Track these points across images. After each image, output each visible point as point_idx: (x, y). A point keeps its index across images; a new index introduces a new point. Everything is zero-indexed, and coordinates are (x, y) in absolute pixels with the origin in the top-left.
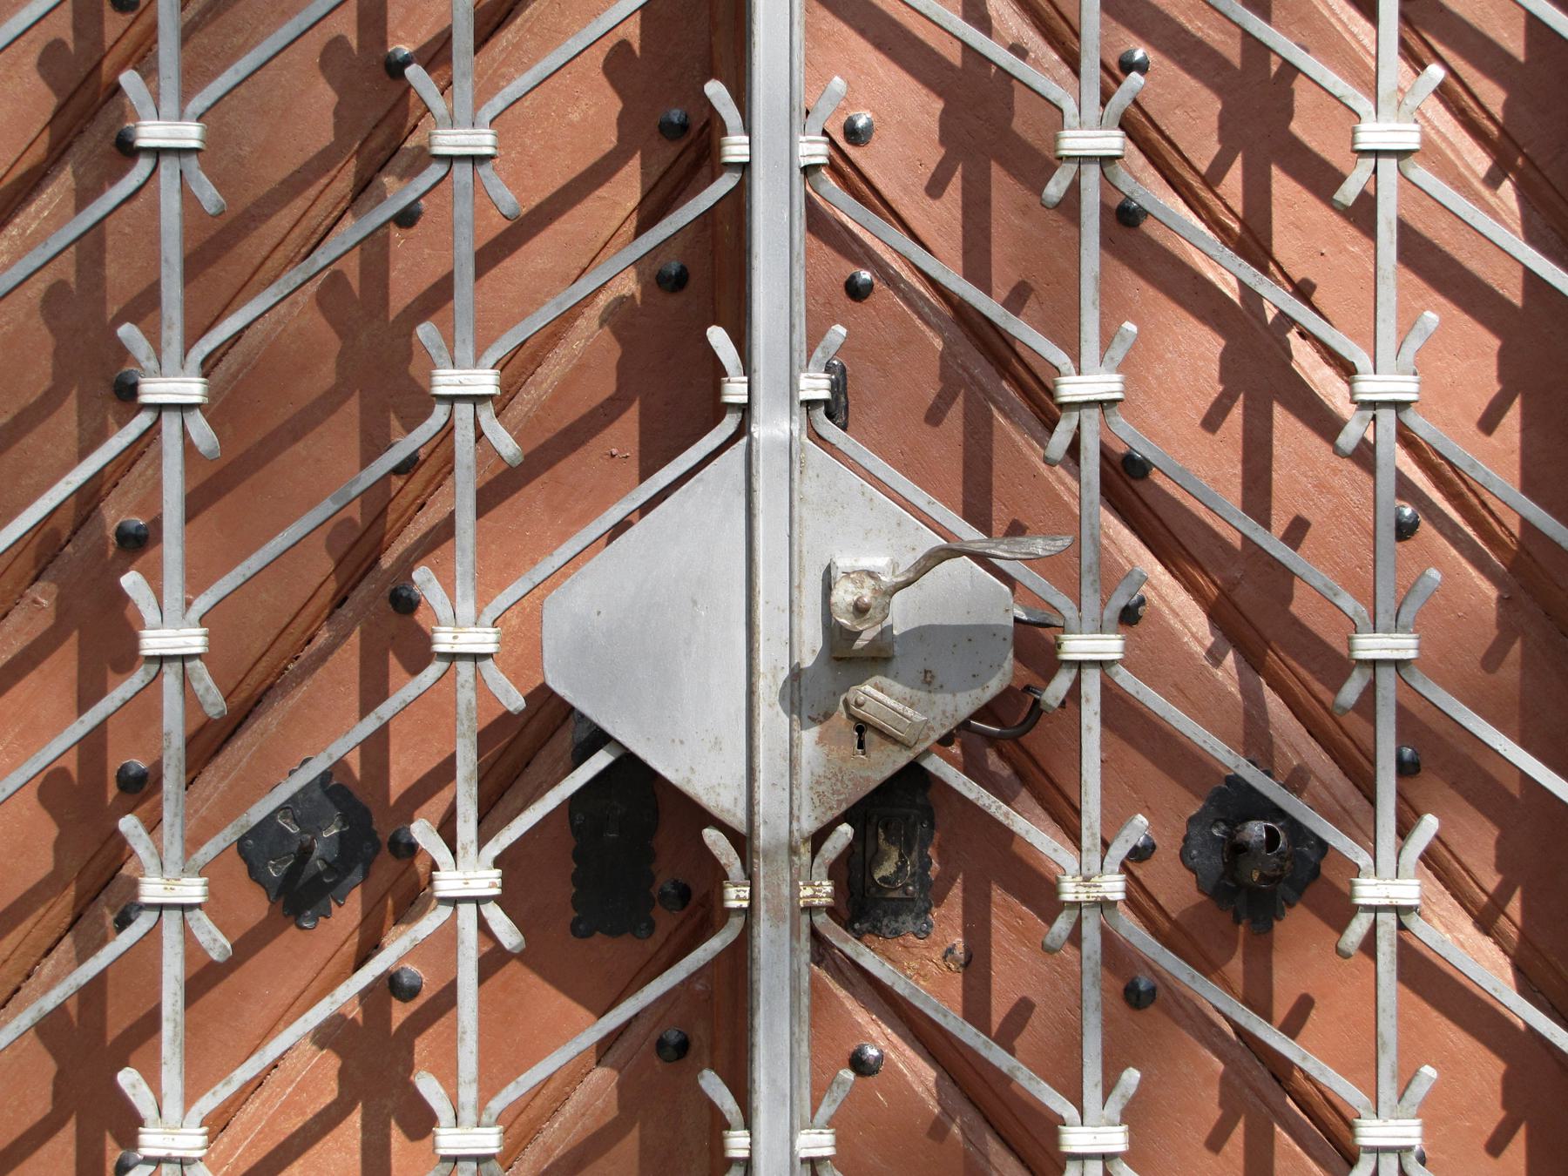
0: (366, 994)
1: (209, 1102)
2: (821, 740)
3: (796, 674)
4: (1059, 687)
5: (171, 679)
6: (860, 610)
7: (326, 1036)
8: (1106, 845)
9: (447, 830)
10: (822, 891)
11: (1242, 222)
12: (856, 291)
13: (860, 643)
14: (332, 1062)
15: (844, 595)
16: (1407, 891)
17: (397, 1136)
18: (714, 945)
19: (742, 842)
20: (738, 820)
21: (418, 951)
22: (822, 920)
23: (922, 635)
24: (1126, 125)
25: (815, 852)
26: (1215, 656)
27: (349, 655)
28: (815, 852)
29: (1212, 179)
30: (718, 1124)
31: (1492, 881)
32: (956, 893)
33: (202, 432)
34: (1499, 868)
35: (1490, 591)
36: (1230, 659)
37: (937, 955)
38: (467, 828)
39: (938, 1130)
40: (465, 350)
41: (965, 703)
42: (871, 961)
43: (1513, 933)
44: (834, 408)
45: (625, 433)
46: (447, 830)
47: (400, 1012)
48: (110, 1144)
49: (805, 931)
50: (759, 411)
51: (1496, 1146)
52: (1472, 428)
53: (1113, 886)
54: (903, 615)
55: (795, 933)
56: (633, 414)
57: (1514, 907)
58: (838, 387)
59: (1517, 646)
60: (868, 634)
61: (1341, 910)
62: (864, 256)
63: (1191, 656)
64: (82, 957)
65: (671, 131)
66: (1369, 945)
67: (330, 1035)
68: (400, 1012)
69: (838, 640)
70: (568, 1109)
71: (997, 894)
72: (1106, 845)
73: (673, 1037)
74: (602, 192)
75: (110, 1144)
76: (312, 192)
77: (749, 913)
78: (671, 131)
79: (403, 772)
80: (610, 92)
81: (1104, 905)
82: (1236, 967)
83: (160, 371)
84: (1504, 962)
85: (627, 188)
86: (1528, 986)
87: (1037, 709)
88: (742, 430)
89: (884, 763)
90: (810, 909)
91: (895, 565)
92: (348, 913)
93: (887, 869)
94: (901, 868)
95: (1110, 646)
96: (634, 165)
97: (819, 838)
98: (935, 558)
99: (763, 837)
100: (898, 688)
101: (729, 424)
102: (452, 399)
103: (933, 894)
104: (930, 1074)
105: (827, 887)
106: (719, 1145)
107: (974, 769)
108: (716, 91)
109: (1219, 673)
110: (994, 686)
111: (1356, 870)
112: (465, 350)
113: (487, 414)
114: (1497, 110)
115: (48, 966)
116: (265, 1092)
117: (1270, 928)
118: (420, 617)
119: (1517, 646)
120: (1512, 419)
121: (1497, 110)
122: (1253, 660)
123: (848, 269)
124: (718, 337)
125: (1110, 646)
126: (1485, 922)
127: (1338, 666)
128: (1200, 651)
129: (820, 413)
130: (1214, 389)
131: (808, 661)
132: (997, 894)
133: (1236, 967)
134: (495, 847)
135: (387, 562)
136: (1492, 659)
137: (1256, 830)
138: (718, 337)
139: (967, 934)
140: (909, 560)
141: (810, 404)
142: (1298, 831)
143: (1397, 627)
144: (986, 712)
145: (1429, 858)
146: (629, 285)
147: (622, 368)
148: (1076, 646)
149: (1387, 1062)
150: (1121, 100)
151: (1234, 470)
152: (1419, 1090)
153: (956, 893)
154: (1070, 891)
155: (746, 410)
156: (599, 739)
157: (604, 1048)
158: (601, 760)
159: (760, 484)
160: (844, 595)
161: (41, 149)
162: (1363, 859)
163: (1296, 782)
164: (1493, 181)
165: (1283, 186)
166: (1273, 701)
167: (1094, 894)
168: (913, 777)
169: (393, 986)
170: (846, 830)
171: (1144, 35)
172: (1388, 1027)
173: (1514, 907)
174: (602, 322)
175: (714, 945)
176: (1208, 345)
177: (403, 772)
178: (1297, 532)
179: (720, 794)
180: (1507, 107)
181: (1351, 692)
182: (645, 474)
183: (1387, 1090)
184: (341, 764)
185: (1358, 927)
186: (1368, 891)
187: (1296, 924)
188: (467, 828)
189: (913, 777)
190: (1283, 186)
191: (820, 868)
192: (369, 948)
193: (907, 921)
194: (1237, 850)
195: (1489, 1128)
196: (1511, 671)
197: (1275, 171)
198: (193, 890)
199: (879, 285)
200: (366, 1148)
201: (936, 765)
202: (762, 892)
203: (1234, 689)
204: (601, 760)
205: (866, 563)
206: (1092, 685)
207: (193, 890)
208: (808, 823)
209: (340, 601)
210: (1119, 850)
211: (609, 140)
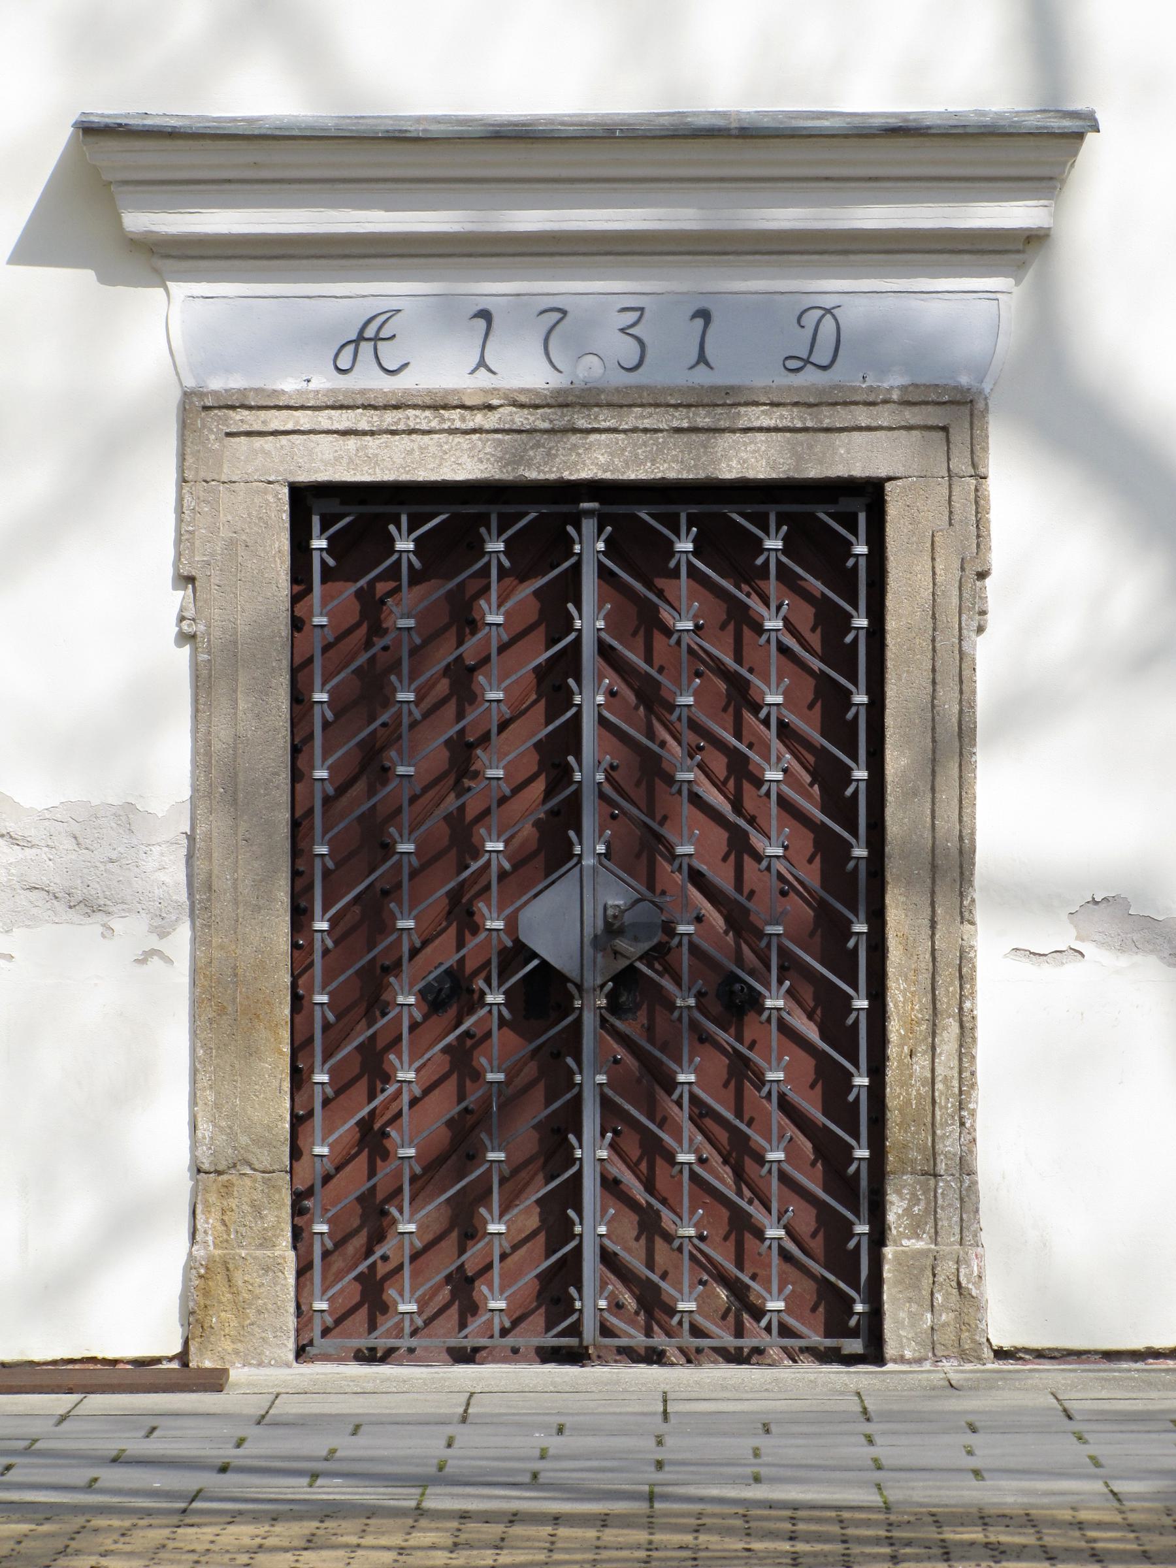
0: (459, 1038)
1: (417, 1064)
2: (603, 956)
3: (596, 936)
4: (676, 941)
5: (405, 936)
6: (615, 917)
7: (445, 1050)
8: (690, 989)
9: (488, 981)
10: (603, 1002)
11: (734, 796)
12: (614, 817)
13: (615, 927)
14: (447, 1058)
15: (610, 912)
16: (780, 1003)
17: (468, 1083)
18: (570, 1019)
19: (579, 987)
20: (578, 980)
21: (475, 1024)
22: (603, 1011)
23: (633, 925)
24: (785, 1227)
25: (601, 990)
26: (726, 933)
27: (452, 931)
28: (601, 990)
29: (725, 783)
30: (571, 1073)
31: (812, 1004)
32: (645, 1006)
33: (414, 860)
34: (814, 1000)
35: (812, 913)
36: (731, 934)
37: (639, 1026)
38: (495, 982)
39: (639, 1081)
40: (494, 836)
41: (646, 946)
42: (618, 1023)
43: (819, 1020)
44: (607, 855)
45: (539, 861)
46: (488, 981)
47: (469, 1043)
48: (378, 1083)
49: (598, 1014)
50: (585, 856)
51: (812, 1086)
52: (805, 862)
53: (692, 1002)
54: (628, 918)
55: (595, 1014)
56: (543, 854)
57: (819, 1012)
58: (608, 848)
59: (819, 931)
60: (617, 924)
61: (761, 1009)
62: (617, 806)
63: (719, 933)
64: (369, 1026)
65: (555, 766)
66: (769, 1020)
67: (447, 1050)
68: (469, 1043)
69: (608, 925)
70: (522, 1074)
71: (658, 1007)
72: (690, 989)
73: (555, 1052)
74: (533, 785)
75: (378, 1083)
76: (442, 783)
77: (581, 1009)
78: (555, 766)
79: (470, 966)
80: (535, 753)
81: (689, 1007)
82: (732, 1030)
83: (402, 843)
84: (816, 1029)
85: (539, 786)
86: (823, 1037)
87: (670, 949)
88: (579, 862)
89: (622, 964)
90: (600, 1008)
91: (625, 903)
92: (452, 1012)
93: (623, 999)
94: (628, 998)
95: (690, 929)
96: (542, 778)
97: (602, 986)
98: (637, 901)
99: (586, 985)
100: (626, 941)
101: (575, 860)
102: (490, 852)
103: (638, 1007)
104: (636, 1064)
105: (605, 1001)
106: (572, 1079)
107: (650, 966)
108: (571, 759)
109: (728, 938)
110: (655, 941)
111: (765, 997)
112: (494, 836)
113: (501, 856)
114: (812, 763)
115: (358, 1027)
116: (427, 1068)
117: (743, 1019)
118: (476, 918)
119: (819, 931)
120: (818, 859)
121: (812, 763)
122: (738, 935)
123: (610, 810)
124: (572, 834)
125: (690, 929)
126: (810, 1017)
127: (760, 934)
128: (721, 931)
129: (603, 857)
130: (725, 849)
131: (599, 932)
132: (658, 1007)
133: (732, 1030)
134: (503, 989)
135: (464, 901)
136: (812, 934)
137: (737, 987)
138: (572, 834)
139: (649, 1020)
140: (630, 902)
141: (600, 854)
142: (751, 988)
143: (409, 841)
144: (653, 949)
145: (788, 992)
146: (542, 815)
147: (539, 840)
148: (682, 929)
149: (774, 1055)
150: (784, 1220)
151: (732, 874)
152: (783, 1064)
153: (645, 1006)
154: (679, 1003)
155: (580, 856)
156: (535, 955)
157: (535, 1052)
158: (535, 962)
159: (585, 878)
160: (610, 912)
161: (357, 770)
162: (767, 994)
163: (751, 973)
164: (811, 785)
165: (746, 786)
166: (745, 948)
167: (687, 1004)
168: (631, 968)
169: (467, 1034)
170: (610, 984)
171: (704, 738)
172: (774, 1044)
173: (819, 1012)
174: (533, 826)
175: (570, 1019)
176: (724, 835)
177: (470, 966)
178: (752, 893)
179: (573, 973)
180: (815, 762)
181: (763, 944)
182: (547, 876)
183: (774, 1063)
184: (451, 966)
185: (766, 1014)
186: (769, 1003)
187: (750, 1018)
188: (495, 982)
189: (631, 968)
190: (746, 786)
191: (603, 995)
192: (459, 1023)
193: (630, 1015)
194: (732, 993)
195: (811, 1081)
196: (818, 938)
197: (744, 781)
198: (412, 1000)
199: (621, 815)
200: (459, 1085)
201: (638, 965)
202: (585, 1002)
203: (732, 943)
204: (535, 962)
205: (617, 903)
206: (685, 940)
207: (412, 1000)
208: (599, 982)
209: (449, 913)
210: (694, 991)
211: (535, 768)
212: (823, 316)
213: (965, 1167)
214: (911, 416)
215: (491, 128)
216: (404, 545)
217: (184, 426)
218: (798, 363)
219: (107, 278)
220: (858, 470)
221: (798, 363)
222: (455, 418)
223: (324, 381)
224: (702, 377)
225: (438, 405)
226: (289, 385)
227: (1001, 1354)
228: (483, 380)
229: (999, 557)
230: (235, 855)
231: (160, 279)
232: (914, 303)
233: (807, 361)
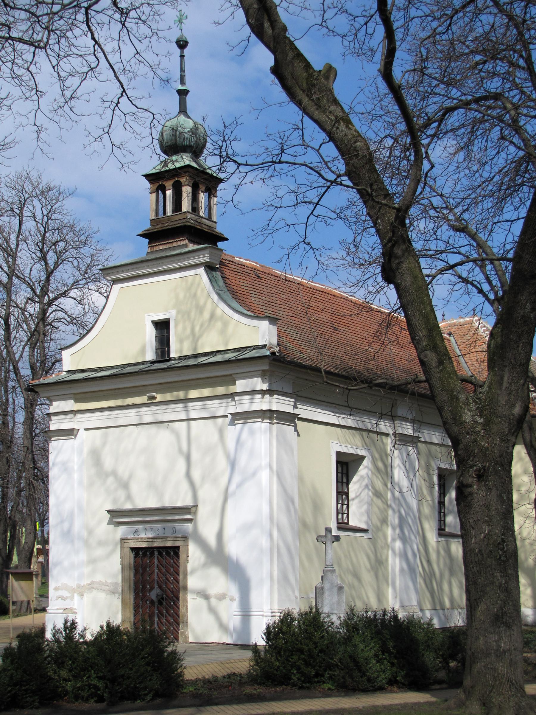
212: (94, 68)
213: (187, 622)
214: (182, 539)
215: (276, 587)
216: (141, 554)
217: (121, 542)
218: (172, 533)
219: (115, 526)
220: (177, 545)
221: (172, 533)
222: (143, 540)
223: (132, 536)
224: (164, 535)
225: (142, 539)
226: (129, 537)
227: (191, 643)
228: (146, 536)
229: (190, 554)
230: (447, 165)
231: (118, 526)
232: (178, 525)
233: (220, 156)
